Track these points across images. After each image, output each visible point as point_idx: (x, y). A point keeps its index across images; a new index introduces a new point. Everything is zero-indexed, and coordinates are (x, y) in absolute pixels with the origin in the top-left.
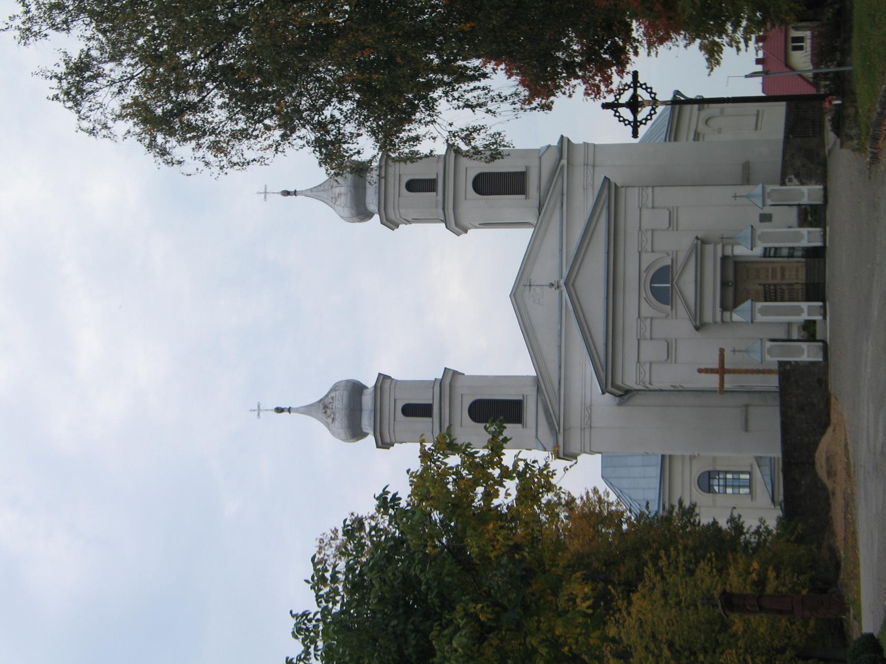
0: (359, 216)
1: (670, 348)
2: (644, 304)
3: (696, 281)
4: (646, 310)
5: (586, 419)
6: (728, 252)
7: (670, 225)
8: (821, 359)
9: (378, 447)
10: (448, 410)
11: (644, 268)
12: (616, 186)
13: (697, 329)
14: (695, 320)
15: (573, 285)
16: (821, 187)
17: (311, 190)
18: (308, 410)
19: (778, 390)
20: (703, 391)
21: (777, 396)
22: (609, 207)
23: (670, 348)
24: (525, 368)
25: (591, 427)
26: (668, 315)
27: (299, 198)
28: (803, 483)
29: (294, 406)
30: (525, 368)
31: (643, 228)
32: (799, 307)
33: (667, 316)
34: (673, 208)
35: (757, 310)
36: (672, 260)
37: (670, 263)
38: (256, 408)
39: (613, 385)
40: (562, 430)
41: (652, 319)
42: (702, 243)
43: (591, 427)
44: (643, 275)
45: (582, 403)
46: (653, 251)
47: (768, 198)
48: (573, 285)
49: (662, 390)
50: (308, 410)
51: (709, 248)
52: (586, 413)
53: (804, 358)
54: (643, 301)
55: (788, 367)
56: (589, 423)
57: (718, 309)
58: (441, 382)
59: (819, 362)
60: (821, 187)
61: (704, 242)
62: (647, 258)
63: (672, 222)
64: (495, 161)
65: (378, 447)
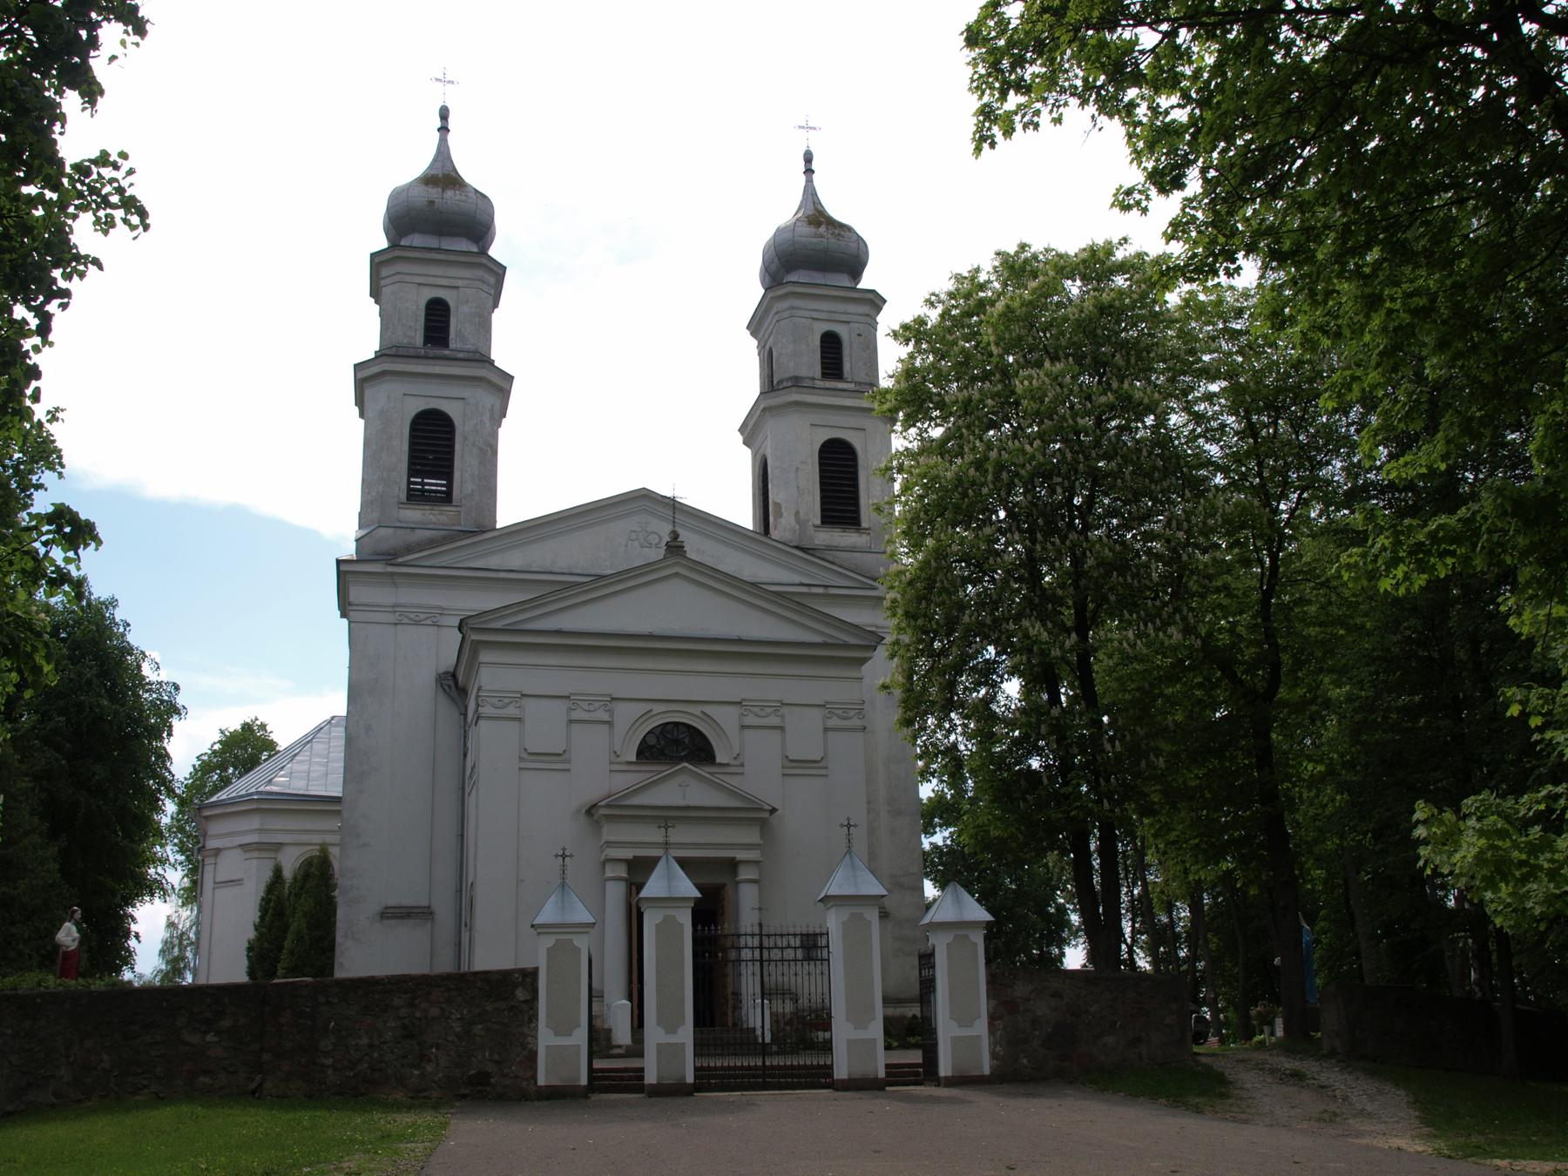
0: (776, 260)
1: (557, 759)
2: (642, 708)
3: (688, 808)
4: (626, 714)
5: (412, 616)
6: (745, 873)
7: (792, 761)
8: (542, 1081)
9: (373, 255)
10: (437, 372)
11: (710, 710)
12: (864, 661)
13: (591, 811)
14: (608, 806)
15: (677, 575)
16: (987, 1071)
17: (814, 194)
18: (443, 153)
19: (464, 969)
20: (462, 835)
21: (444, 966)
22: (824, 645)
23: (557, 759)
24: (511, 509)
25: (396, 624)
26: (618, 756)
27: (803, 178)
28: (210, 1038)
29: (451, 138)
30: (511, 509)
31: (785, 710)
32: (682, 1021)
33: (615, 752)
34: (826, 768)
35: (671, 912)
36: (728, 765)
37: (718, 760)
38: (448, 78)
39: (477, 646)
40: (390, 569)
41: (610, 723)
42: (759, 816)
43: (396, 624)
44: (696, 710)
45: (443, 609)
46: (743, 727)
47: (956, 936)
48: (677, 575)
49: (465, 755)
50: (443, 153)
51: (751, 835)
52: (422, 616)
53: (546, 1039)
54: (645, 707)
55: (521, 994)
56: (406, 621)
57: (629, 854)
58: (487, 361)
59: (534, 1077)
60: (987, 1071)
61: (763, 825)
62: (727, 718)
63: (795, 767)
64: (1063, 252)
65: (373, 255)
